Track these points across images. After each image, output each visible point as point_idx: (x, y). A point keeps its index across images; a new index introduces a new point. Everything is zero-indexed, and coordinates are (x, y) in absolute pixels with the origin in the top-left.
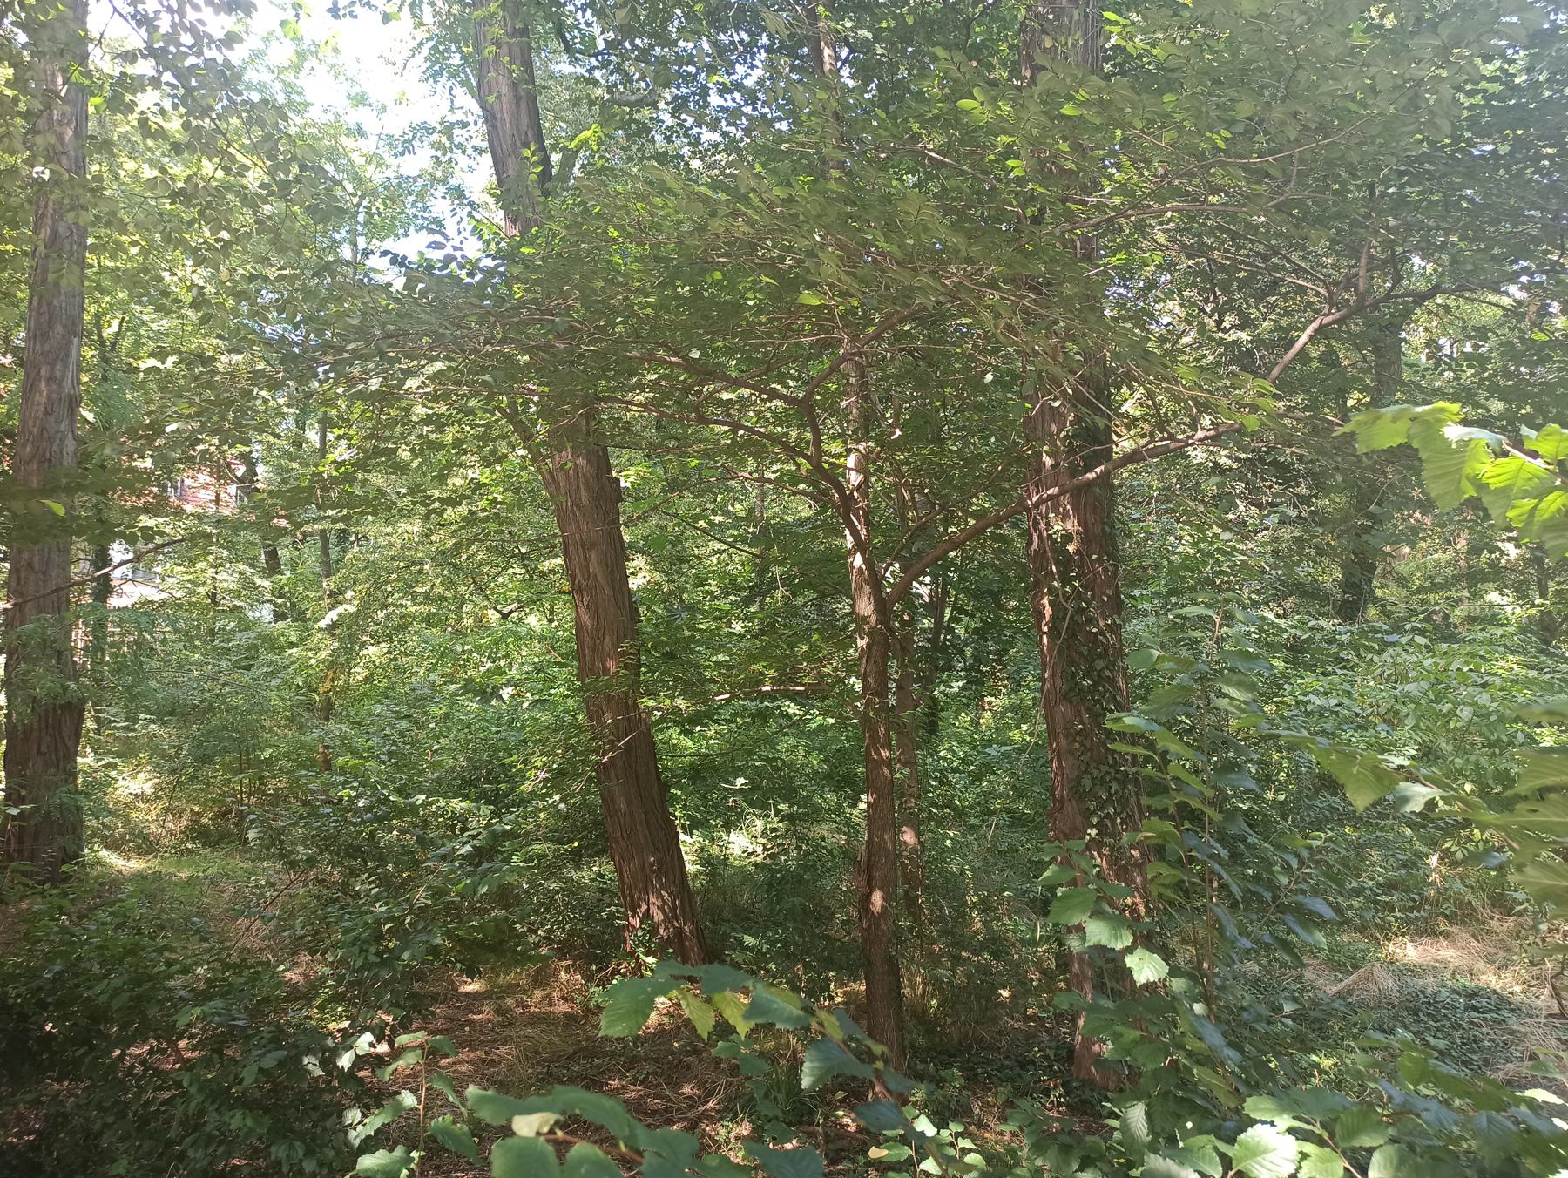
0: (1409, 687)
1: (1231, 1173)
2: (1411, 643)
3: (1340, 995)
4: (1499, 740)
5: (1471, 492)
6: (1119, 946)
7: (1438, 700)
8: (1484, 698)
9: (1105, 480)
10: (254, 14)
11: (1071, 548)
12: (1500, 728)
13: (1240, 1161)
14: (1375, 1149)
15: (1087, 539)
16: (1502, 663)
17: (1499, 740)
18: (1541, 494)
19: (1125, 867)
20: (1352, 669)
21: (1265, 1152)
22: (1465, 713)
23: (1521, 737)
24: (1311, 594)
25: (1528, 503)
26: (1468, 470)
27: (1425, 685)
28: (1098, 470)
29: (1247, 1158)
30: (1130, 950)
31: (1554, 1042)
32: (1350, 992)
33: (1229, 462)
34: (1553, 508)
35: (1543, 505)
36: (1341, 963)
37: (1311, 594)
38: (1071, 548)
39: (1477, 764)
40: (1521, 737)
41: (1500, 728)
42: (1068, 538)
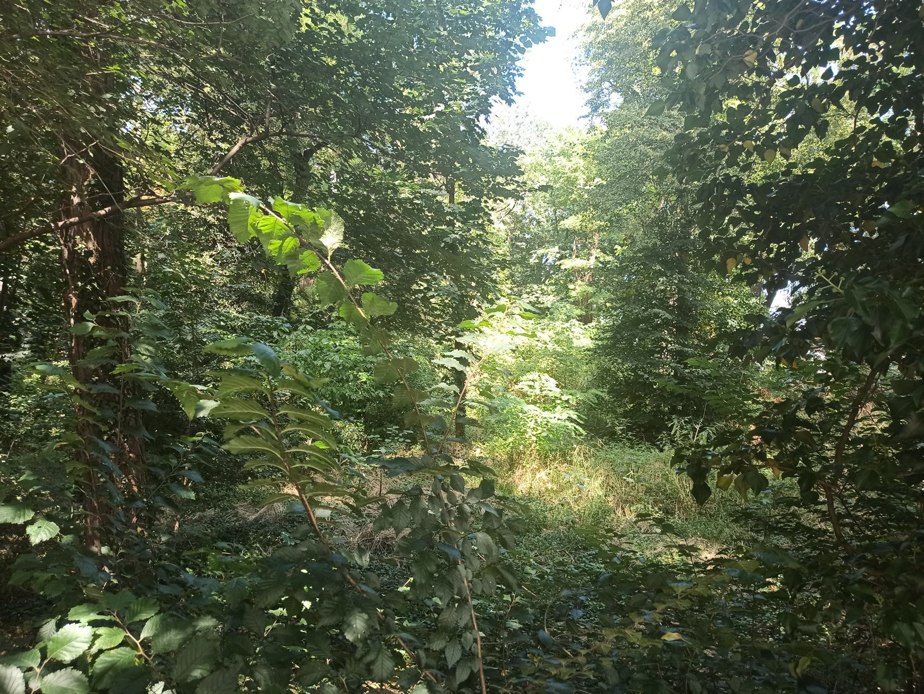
0: (302, 352)
1: (46, 661)
2: (304, 329)
3: (256, 520)
4: (342, 379)
5: (254, 234)
6: (21, 521)
7: (315, 359)
8: (336, 358)
9: (116, 216)
10: (521, 161)
11: (92, 260)
12: (343, 372)
13: (53, 651)
14: (147, 620)
15: (103, 255)
16: (347, 341)
17: (342, 379)
18: (283, 238)
19: (125, 465)
20: (276, 342)
21: (70, 641)
22: (328, 365)
23: (351, 376)
24: (258, 302)
25: (277, 243)
26: (250, 221)
27: (309, 351)
28: (107, 209)
29: (57, 648)
30: (32, 522)
31: (352, 524)
32: (261, 517)
33: (213, 220)
34: (290, 246)
35: (285, 244)
36: (256, 501)
37: (258, 302)
38: (92, 260)
39: (332, 392)
40: (351, 376)
41: (343, 372)
42: (89, 253)
